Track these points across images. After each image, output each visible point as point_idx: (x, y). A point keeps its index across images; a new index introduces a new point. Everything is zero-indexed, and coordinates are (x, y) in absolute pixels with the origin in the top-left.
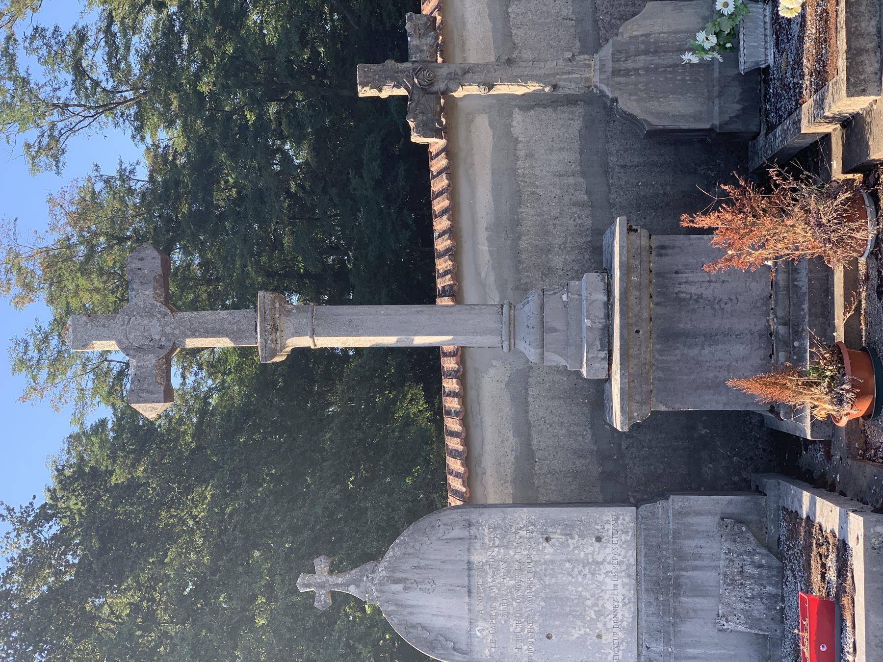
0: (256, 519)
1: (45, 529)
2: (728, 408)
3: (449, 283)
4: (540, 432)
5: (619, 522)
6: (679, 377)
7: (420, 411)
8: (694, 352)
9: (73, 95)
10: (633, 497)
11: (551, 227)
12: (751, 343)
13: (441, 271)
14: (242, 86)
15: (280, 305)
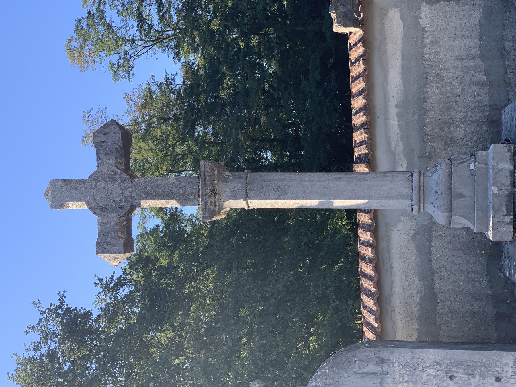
1: (120, 292)
3: (364, 152)
4: (442, 278)
7: (344, 225)
9: (138, 33)
11: (453, 104)
13: (358, 142)
14: (237, 25)
15: (219, 172)
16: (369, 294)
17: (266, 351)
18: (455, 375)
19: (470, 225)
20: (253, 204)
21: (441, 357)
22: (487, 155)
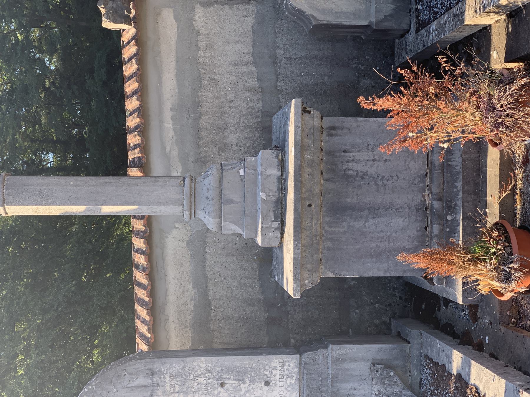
0: (18, 304)
2: (388, 275)
5: (285, 368)
6: (345, 247)
8: (359, 224)
10: (294, 338)
11: (227, 109)
12: (409, 216)
13: (132, 145)
16: (143, 304)
17: (45, 367)
18: (226, 382)
19: (240, 232)
20: (12, 211)
21: (212, 364)
22: (256, 161)
